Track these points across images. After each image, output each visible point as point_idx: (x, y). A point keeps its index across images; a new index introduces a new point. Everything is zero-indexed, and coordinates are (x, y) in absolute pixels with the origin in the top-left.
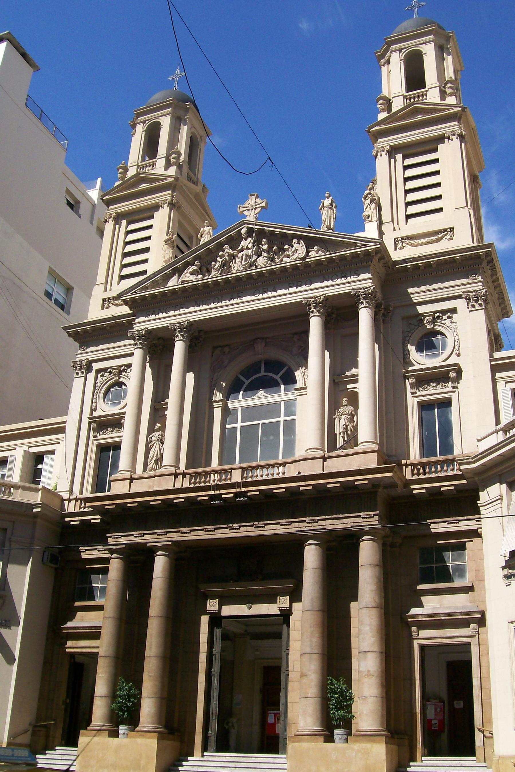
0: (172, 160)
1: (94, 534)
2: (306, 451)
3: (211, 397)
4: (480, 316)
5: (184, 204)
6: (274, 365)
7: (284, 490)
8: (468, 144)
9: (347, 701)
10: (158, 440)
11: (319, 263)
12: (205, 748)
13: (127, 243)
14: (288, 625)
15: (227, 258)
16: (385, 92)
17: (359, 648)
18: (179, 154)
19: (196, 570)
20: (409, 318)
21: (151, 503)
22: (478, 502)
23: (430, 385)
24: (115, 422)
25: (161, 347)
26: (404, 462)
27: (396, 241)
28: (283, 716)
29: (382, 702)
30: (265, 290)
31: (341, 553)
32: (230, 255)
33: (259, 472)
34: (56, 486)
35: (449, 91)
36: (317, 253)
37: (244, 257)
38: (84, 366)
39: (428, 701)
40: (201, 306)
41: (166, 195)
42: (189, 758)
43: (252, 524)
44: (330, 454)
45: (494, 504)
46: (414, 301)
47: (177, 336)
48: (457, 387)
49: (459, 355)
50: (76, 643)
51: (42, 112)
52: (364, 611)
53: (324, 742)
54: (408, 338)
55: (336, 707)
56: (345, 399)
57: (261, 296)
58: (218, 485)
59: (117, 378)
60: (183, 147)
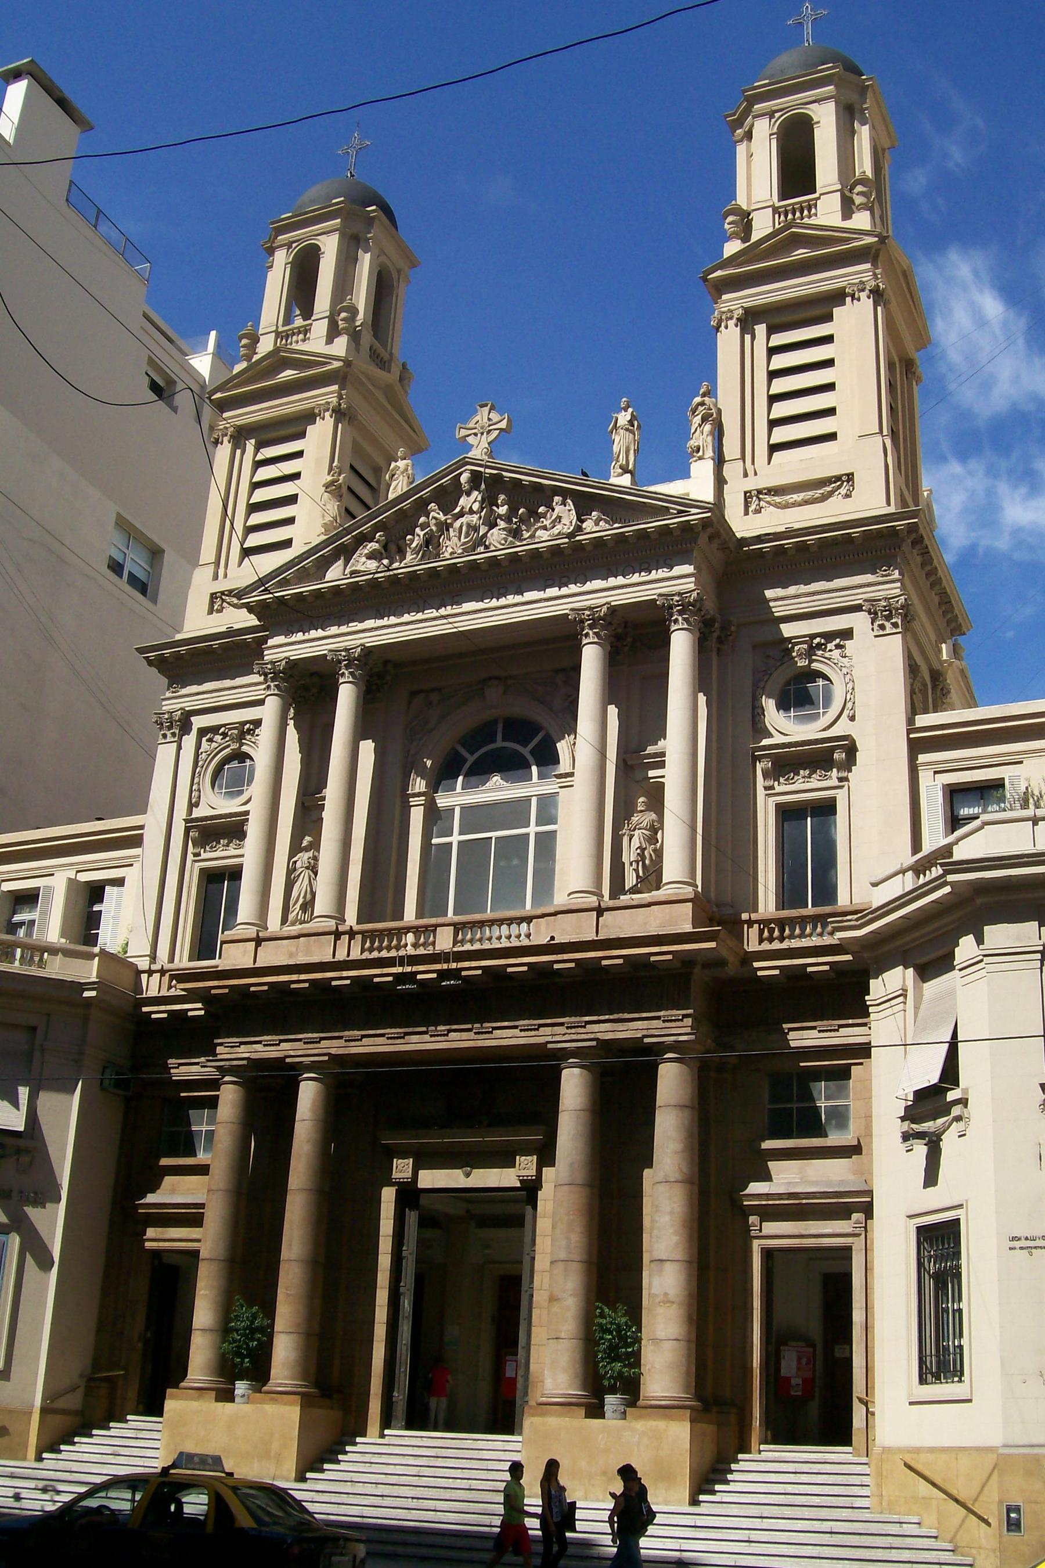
0: (340, 322)
1: (192, 1036)
2: (569, 895)
3: (405, 786)
5: (365, 412)
6: (521, 729)
8: (893, 306)
9: (632, 1344)
10: (307, 868)
11: (599, 542)
12: (386, 1422)
13: (256, 486)
14: (535, 1207)
15: (434, 528)
16: (742, 200)
18: (353, 311)
19: (376, 1109)
21: (293, 986)
22: (867, 998)
24: (232, 829)
25: (314, 691)
26: (745, 916)
27: (747, 496)
29: (689, 1349)
30: (502, 591)
31: (624, 1085)
33: (496, 931)
34: (127, 944)
35: (858, 200)
36: (597, 524)
37: (464, 528)
41: (328, 395)
42: (358, 1440)
43: (469, 1026)
44: (612, 903)
45: (893, 1002)
47: (587, 635)
48: (846, 779)
49: (852, 718)
51: (99, 211)
53: (586, 1417)
54: (761, 685)
56: (641, 799)
57: (494, 603)
58: (410, 957)
59: (235, 746)
60: (361, 297)
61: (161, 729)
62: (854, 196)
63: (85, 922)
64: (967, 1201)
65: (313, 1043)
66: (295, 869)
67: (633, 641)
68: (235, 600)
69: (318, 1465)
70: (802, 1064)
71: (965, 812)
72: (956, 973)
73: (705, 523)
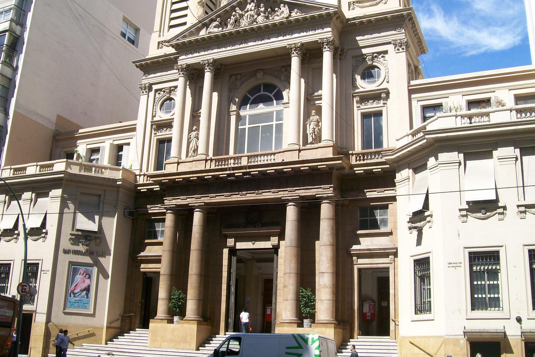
1: (156, 197)
4: (403, 56)
6: (269, 87)
7: (274, 171)
9: (311, 302)
11: (297, 20)
13: (172, 19)
14: (277, 255)
19: (221, 221)
20: (357, 56)
24: (168, 125)
26: (350, 152)
31: (309, 210)
32: (240, 15)
36: (296, 14)
37: (249, 16)
42: (217, 336)
44: (304, 148)
48: (386, 104)
49: (388, 82)
52: (323, 247)
54: (355, 70)
56: (314, 111)
57: (260, 42)
59: (168, 95)
63: (117, 159)
67: (311, 55)
68: (167, 44)
71: (428, 115)
72: (427, 171)
73: (335, 13)
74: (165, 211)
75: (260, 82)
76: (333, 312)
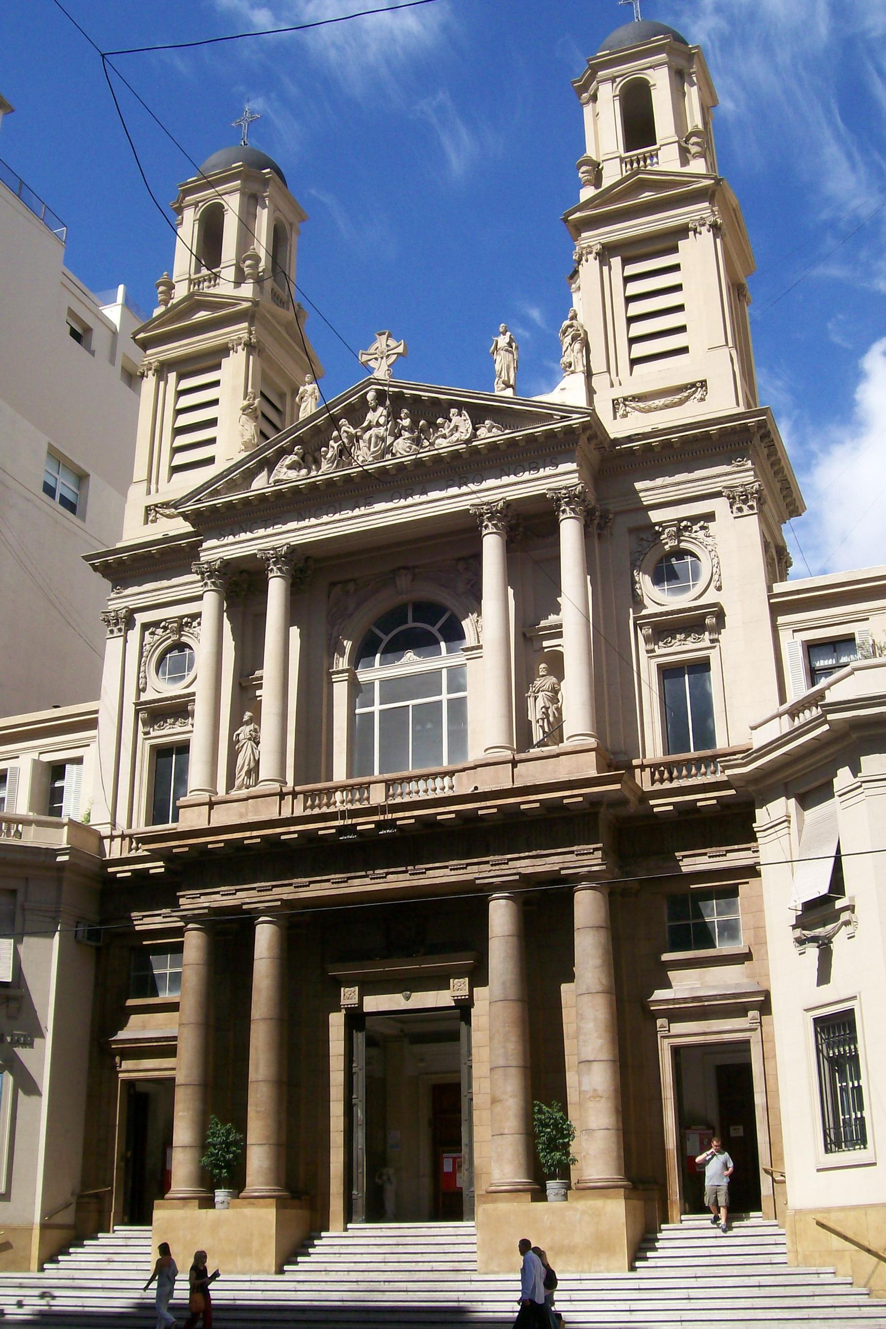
0: (245, 269)
1: (155, 891)
4: (752, 525)
5: (273, 349)
6: (428, 611)
8: (728, 238)
10: (249, 739)
11: (493, 447)
12: (349, 1217)
14: (469, 1023)
16: (591, 152)
17: (578, 1054)
18: (257, 259)
19: (324, 945)
21: (246, 842)
22: (754, 825)
23: (675, 638)
24: (180, 709)
25: (245, 586)
26: (635, 762)
27: (615, 403)
28: (467, 1163)
29: (618, 1136)
31: (545, 912)
33: (413, 786)
34: (89, 814)
35: (694, 149)
38: (122, 618)
39: (689, 1128)
40: (307, 520)
41: (240, 331)
42: (323, 1234)
44: (523, 756)
45: (777, 828)
46: (645, 503)
47: (272, 570)
48: (717, 640)
49: (719, 589)
50: (136, 1064)
51: (22, 182)
52: (585, 998)
54: (638, 563)
55: (548, 1145)
56: (542, 666)
57: (403, 502)
58: (350, 811)
61: (108, 626)
62: (690, 146)
63: (50, 798)
64: (860, 993)
65: (266, 890)
66: (238, 741)
67: (530, 530)
69: (293, 1259)
70: (692, 886)
73: (585, 426)
74: (182, 924)
75: (404, 598)
76: (619, 1157)
